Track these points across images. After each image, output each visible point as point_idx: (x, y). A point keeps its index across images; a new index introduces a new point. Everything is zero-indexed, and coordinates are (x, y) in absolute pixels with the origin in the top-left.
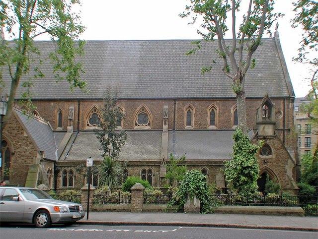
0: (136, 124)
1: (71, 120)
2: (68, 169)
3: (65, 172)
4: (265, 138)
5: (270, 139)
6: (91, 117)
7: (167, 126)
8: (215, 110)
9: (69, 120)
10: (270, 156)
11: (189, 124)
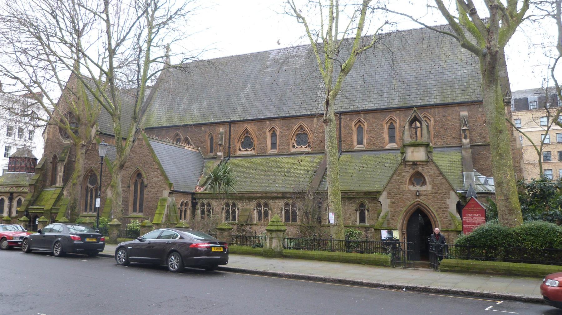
0: (294, 147)
1: (220, 145)
2: (205, 202)
3: (203, 205)
4: (415, 164)
5: (423, 165)
6: (243, 140)
7: (468, 140)
8: (394, 124)
9: (218, 146)
10: (424, 188)
11: (360, 142)
